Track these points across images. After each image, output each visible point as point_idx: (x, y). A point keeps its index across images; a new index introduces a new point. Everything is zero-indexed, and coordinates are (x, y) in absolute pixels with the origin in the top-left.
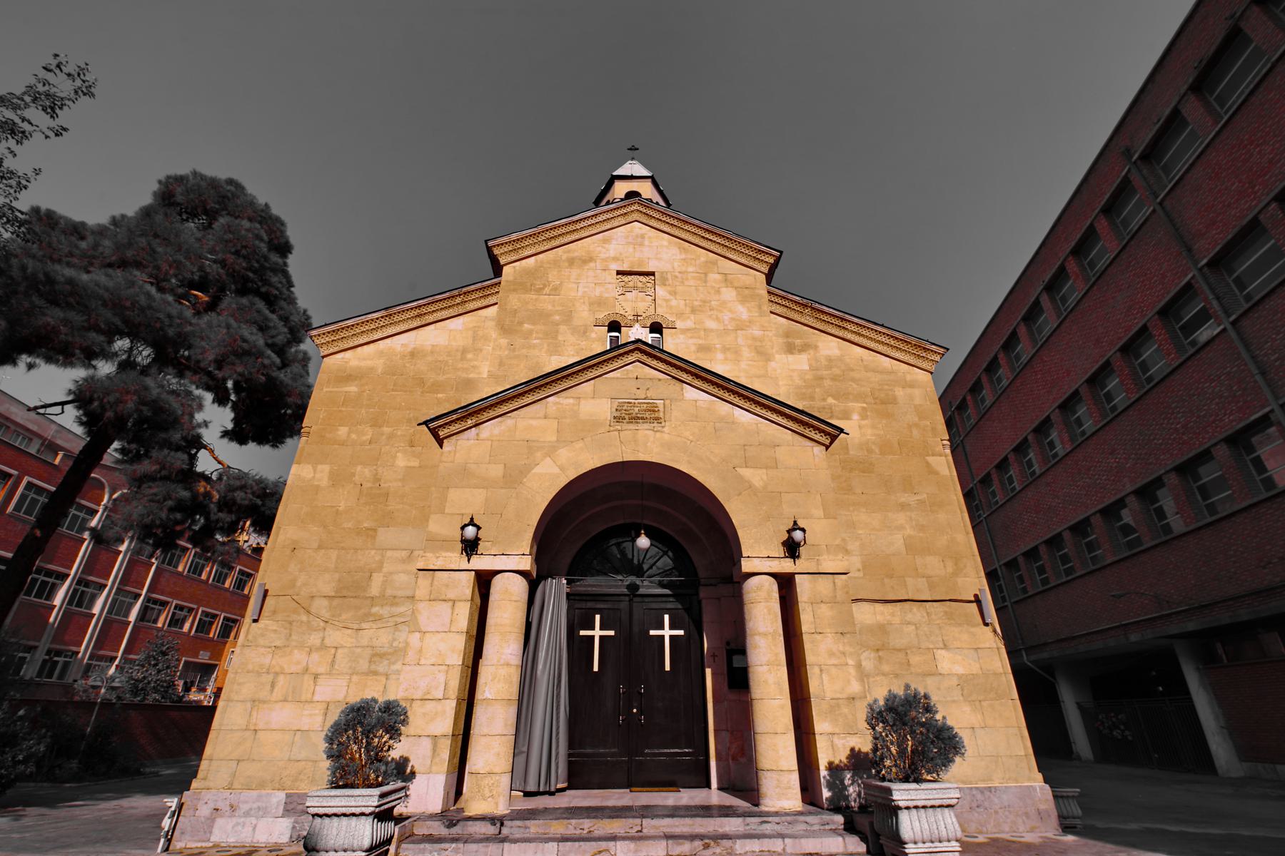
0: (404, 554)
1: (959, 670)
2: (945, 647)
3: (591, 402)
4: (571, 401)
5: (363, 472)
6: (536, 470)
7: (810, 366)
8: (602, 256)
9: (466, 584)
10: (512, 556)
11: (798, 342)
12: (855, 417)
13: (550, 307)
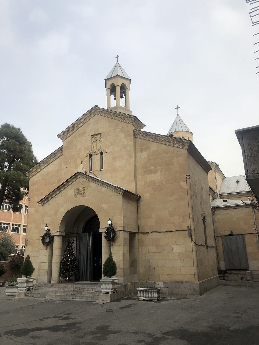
3: (70, 191)
12: (159, 172)
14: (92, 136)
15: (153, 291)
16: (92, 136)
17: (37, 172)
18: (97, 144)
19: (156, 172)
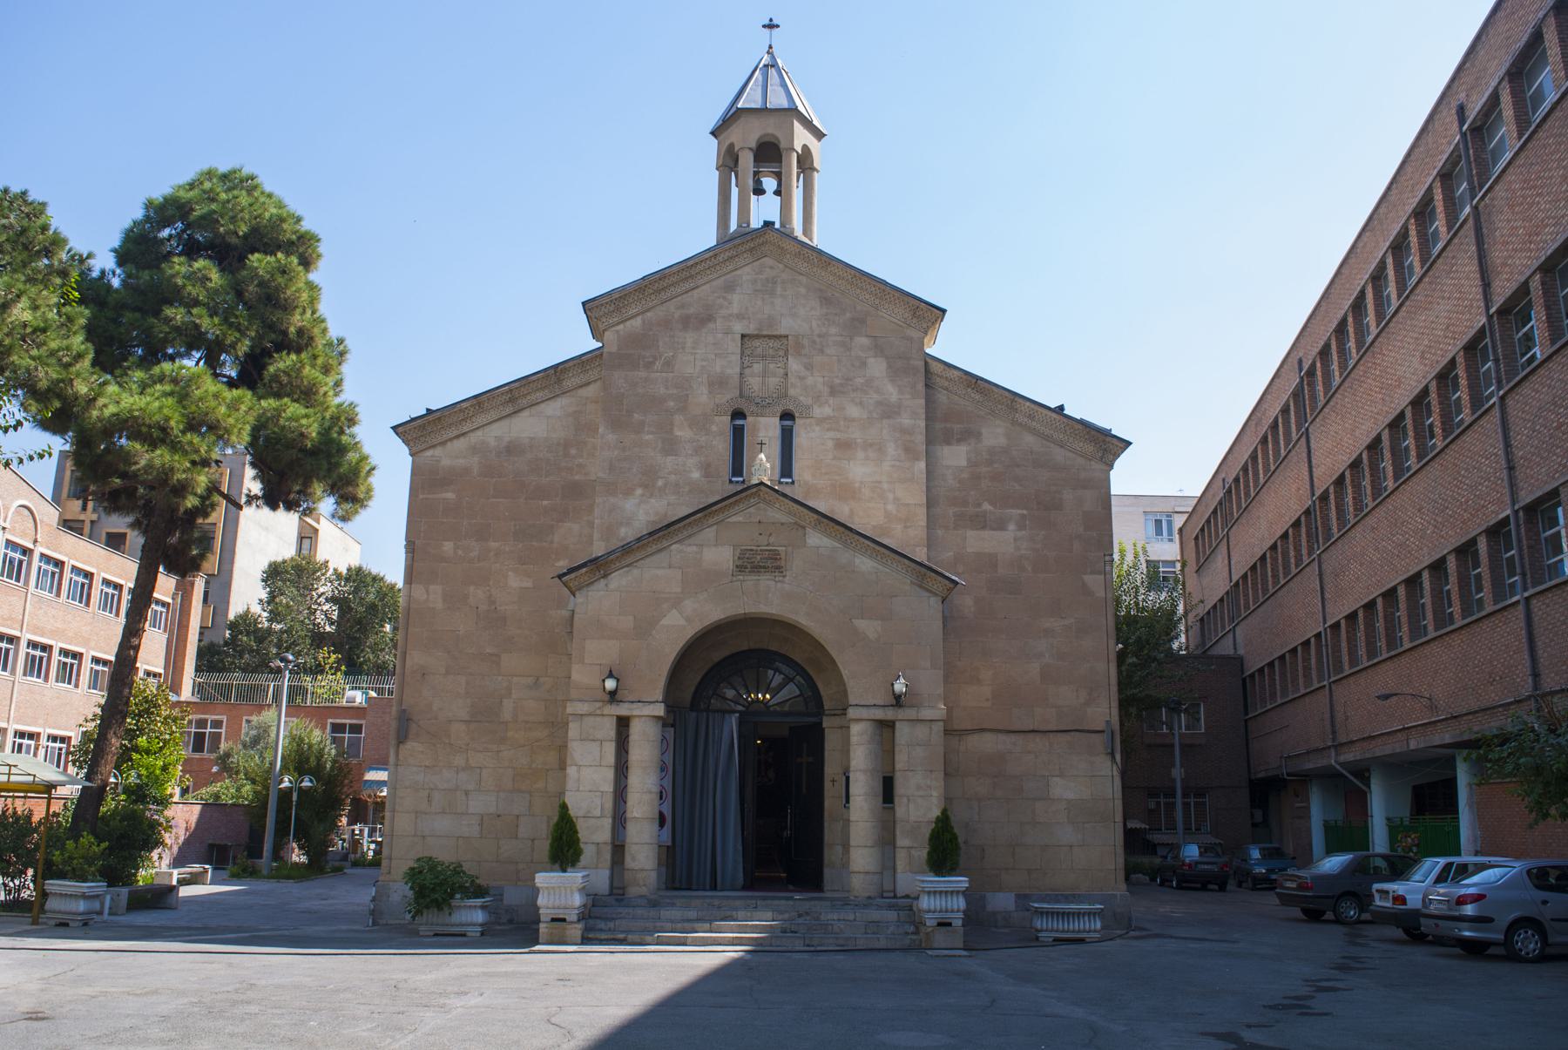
0: (530, 680)
1: (1070, 795)
2: (1061, 776)
4: (695, 548)
5: (477, 594)
6: (664, 622)
7: (969, 460)
8: (724, 312)
9: (609, 729)
10: (646, 714)
11: (957, 427)
12: (1012, 527)
13: (662, 391)
14: (743, 336)
15: (1090, 914)
16: (743, 336)
17: (456, 433)
18: (765, 374)
19: (1000, 525)
